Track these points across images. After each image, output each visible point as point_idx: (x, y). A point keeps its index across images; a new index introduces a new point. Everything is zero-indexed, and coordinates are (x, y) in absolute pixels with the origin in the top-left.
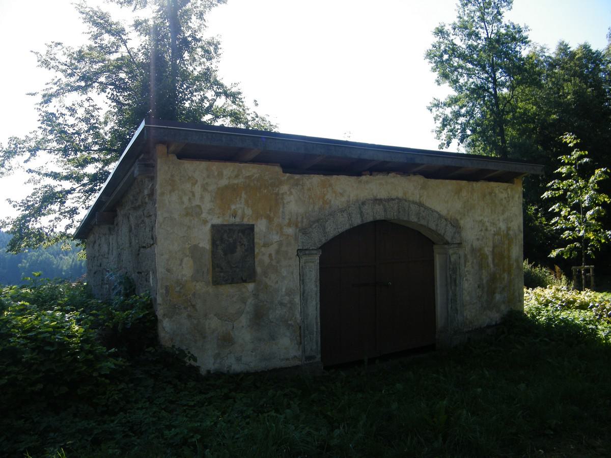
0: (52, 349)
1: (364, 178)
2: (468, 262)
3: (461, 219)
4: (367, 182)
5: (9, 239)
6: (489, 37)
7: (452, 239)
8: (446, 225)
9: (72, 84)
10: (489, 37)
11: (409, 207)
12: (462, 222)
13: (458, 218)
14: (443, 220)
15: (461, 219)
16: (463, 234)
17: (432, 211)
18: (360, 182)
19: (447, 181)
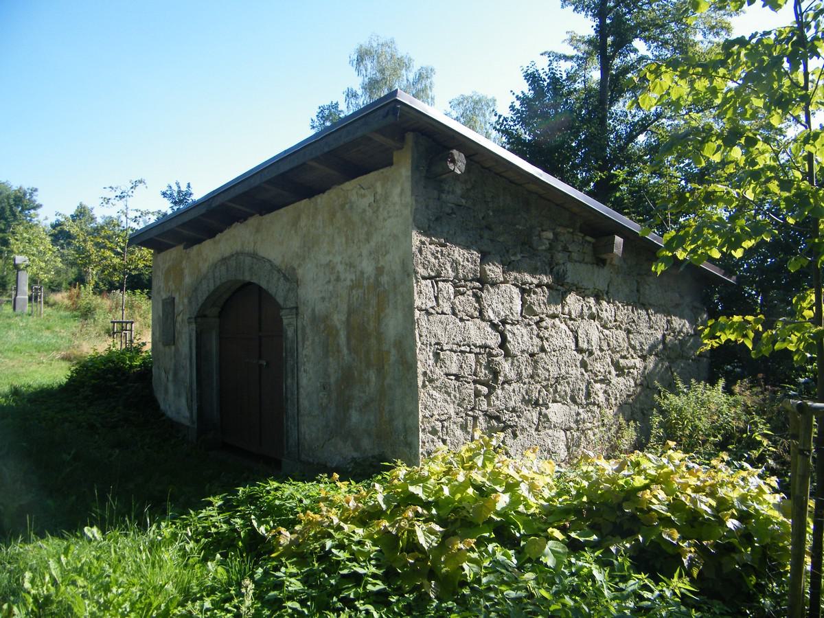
3: (299, 265)
7: (285, 300)
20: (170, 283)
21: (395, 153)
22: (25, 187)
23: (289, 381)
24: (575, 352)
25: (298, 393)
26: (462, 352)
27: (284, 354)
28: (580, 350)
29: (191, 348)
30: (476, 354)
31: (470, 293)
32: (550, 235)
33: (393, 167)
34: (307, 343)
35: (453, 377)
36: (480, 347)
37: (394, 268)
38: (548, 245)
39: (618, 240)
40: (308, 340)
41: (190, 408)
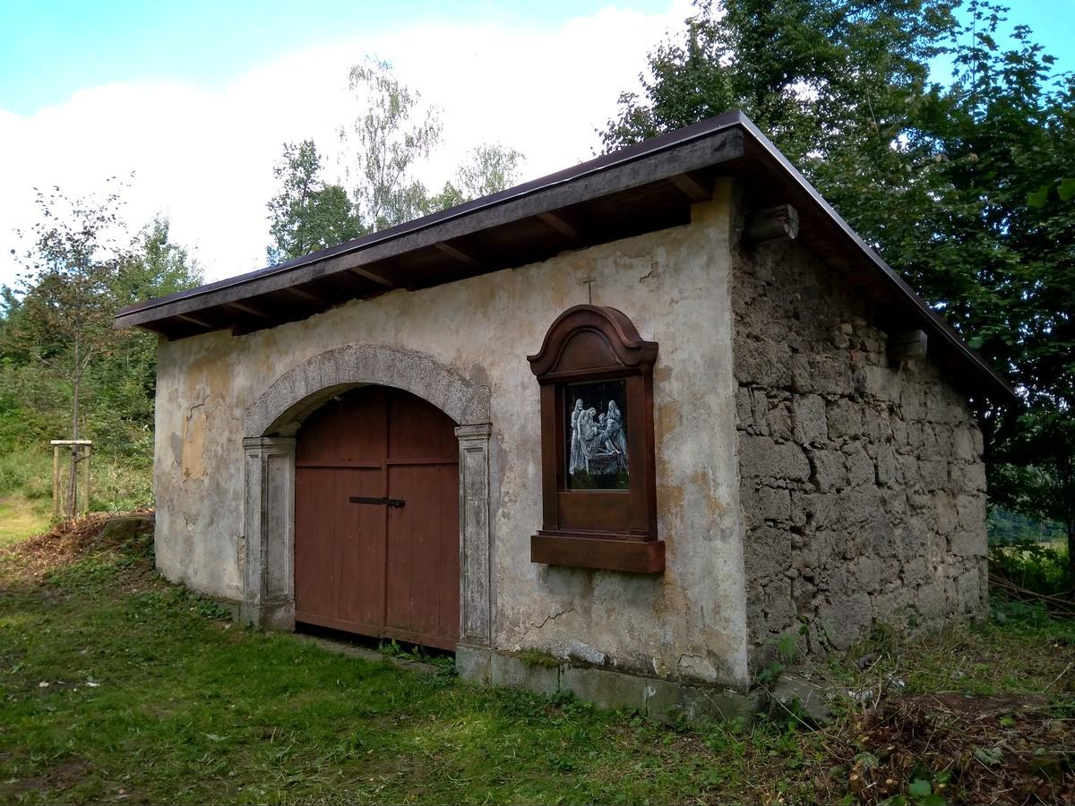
0: (259, 596)
1: (312, 319)
2: (511, 469)
3: (492, 365)
4: (316, 326)
5: (638, 588)
6: (1038, 72)
7: (464, 413)
8: (450, 384)
9: (605, 433)
10: (1038, 72)
11: (375, 355)
12: (494, 374)
13: (485, 365)
14: (444, 373)
15: (492, 365)
16: (497, 403)
17: (420, 358)
18: (307, 327)
19: (455, 285)
20: (842, 346)
21: (693, 207)
22: (276, 188)
23: (470, 529)
24: (875, 486)
25: (489, 554)
26: (779, 487)
27: (461, 492)
28: (879, 484)
29: (247, 482)
30: (791, 490)
31: (781, 405)
32: (848, 328)
33: (690, 228)
34: (510, 475)
35: (772, 524)
36: (794, 480)
37: (691, 370)
38: (848, 343)
39: (923, 336)
40: (511, 469)
41: (244, 575)
